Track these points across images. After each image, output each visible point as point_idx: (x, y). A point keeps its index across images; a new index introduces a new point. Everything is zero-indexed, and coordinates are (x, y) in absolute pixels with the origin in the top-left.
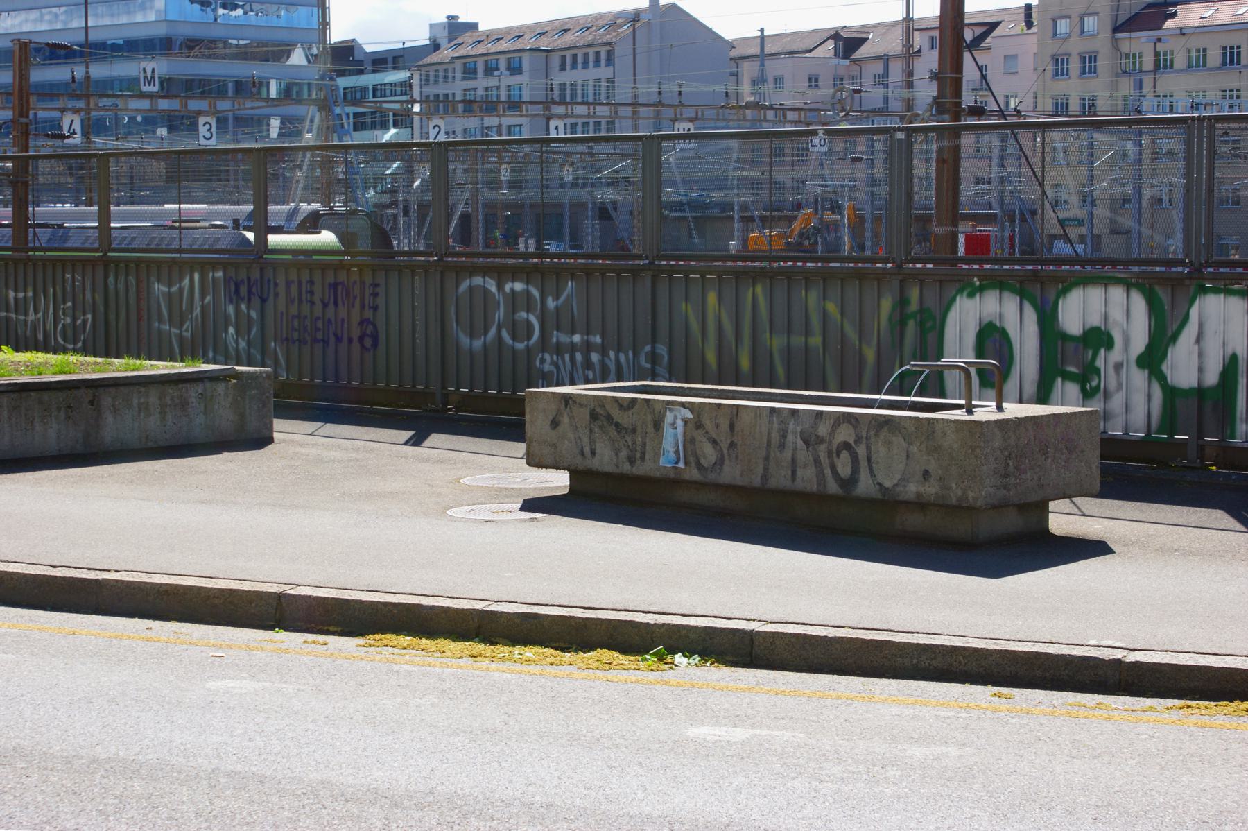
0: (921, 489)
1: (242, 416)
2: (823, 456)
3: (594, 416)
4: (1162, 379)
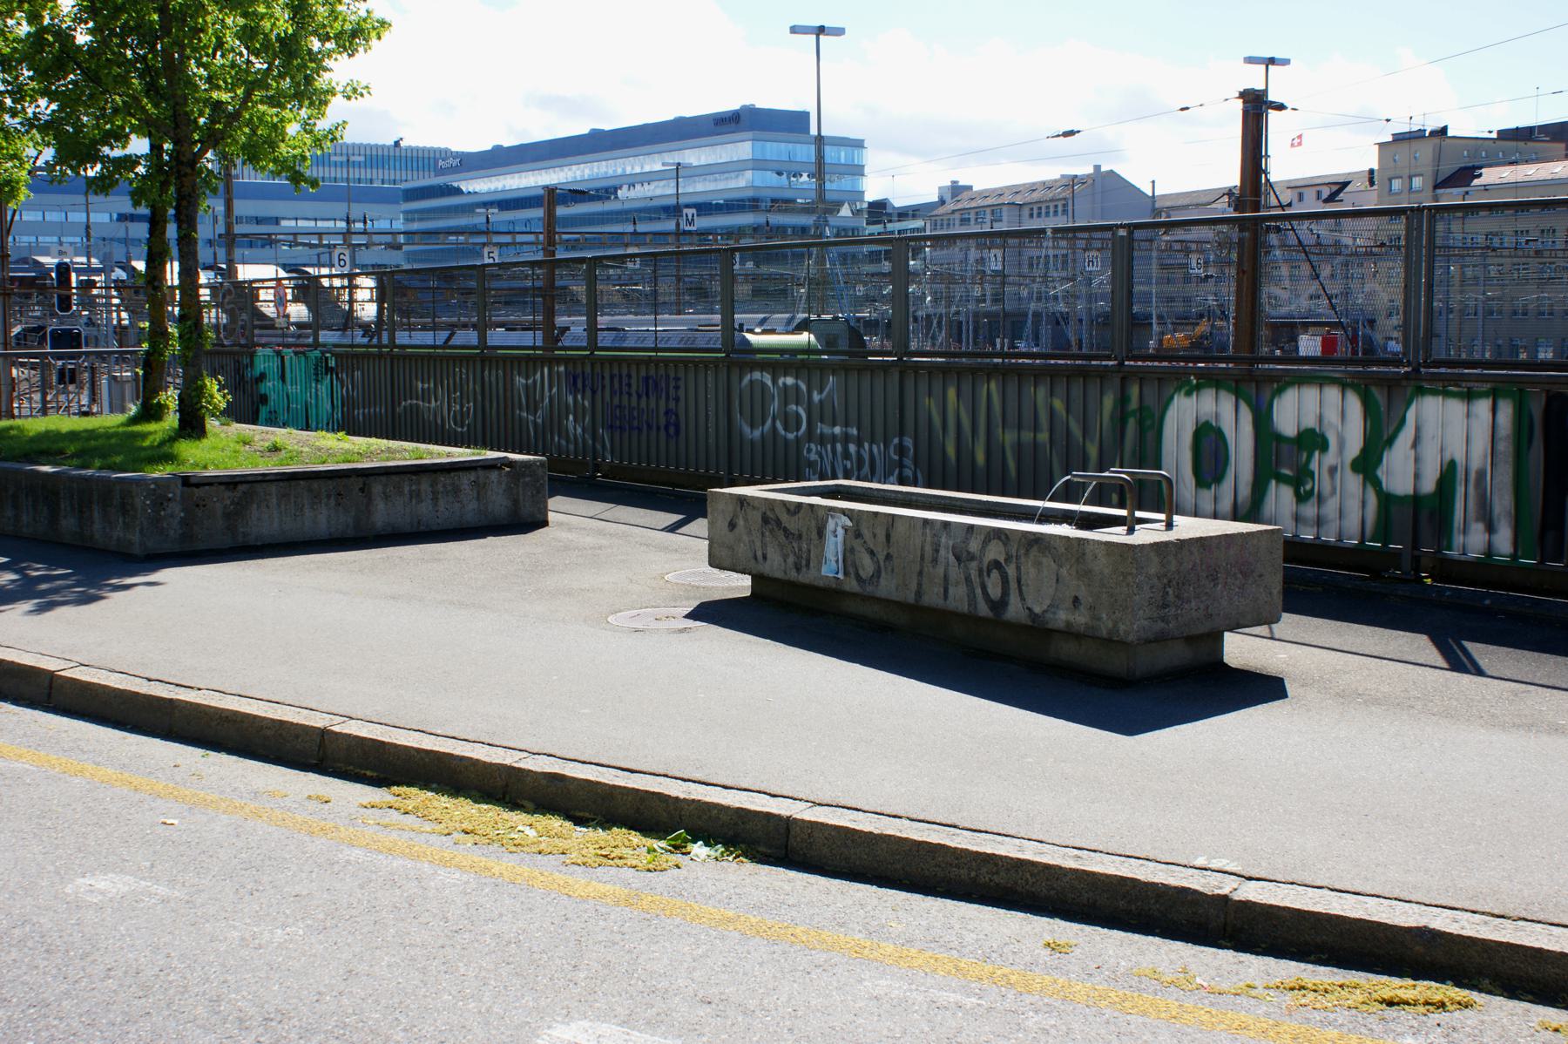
0: (1071, 618)
1: (516, 502)
2: (974, 574)
3: (765, 520)
4: (1377, 484)
